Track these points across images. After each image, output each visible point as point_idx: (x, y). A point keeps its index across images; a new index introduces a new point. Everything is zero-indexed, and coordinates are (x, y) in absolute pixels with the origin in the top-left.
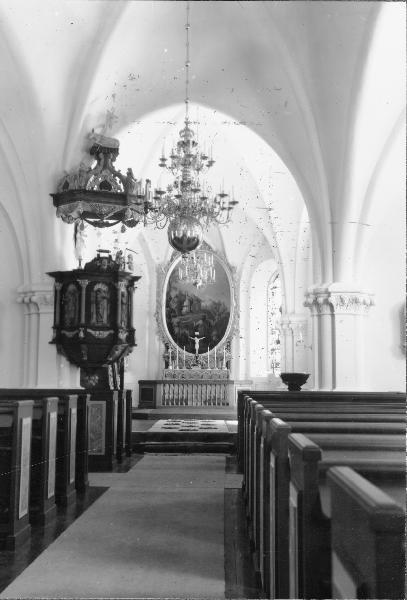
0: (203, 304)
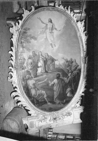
0: (57, 63)
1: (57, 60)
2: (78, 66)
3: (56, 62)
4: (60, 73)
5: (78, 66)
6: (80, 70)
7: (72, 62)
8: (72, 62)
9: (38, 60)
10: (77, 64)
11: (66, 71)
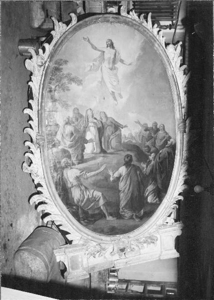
0: (124, 132)
1: (126, 126)
2: (170, 138)
3: (123, 130)
4: (129, 153)
5: (170, 138)
6: (174, 147)
7: (158, 130)
8: (158, 130)
9: (86, 128)
10: (167, 133)
11: (144, 149)
